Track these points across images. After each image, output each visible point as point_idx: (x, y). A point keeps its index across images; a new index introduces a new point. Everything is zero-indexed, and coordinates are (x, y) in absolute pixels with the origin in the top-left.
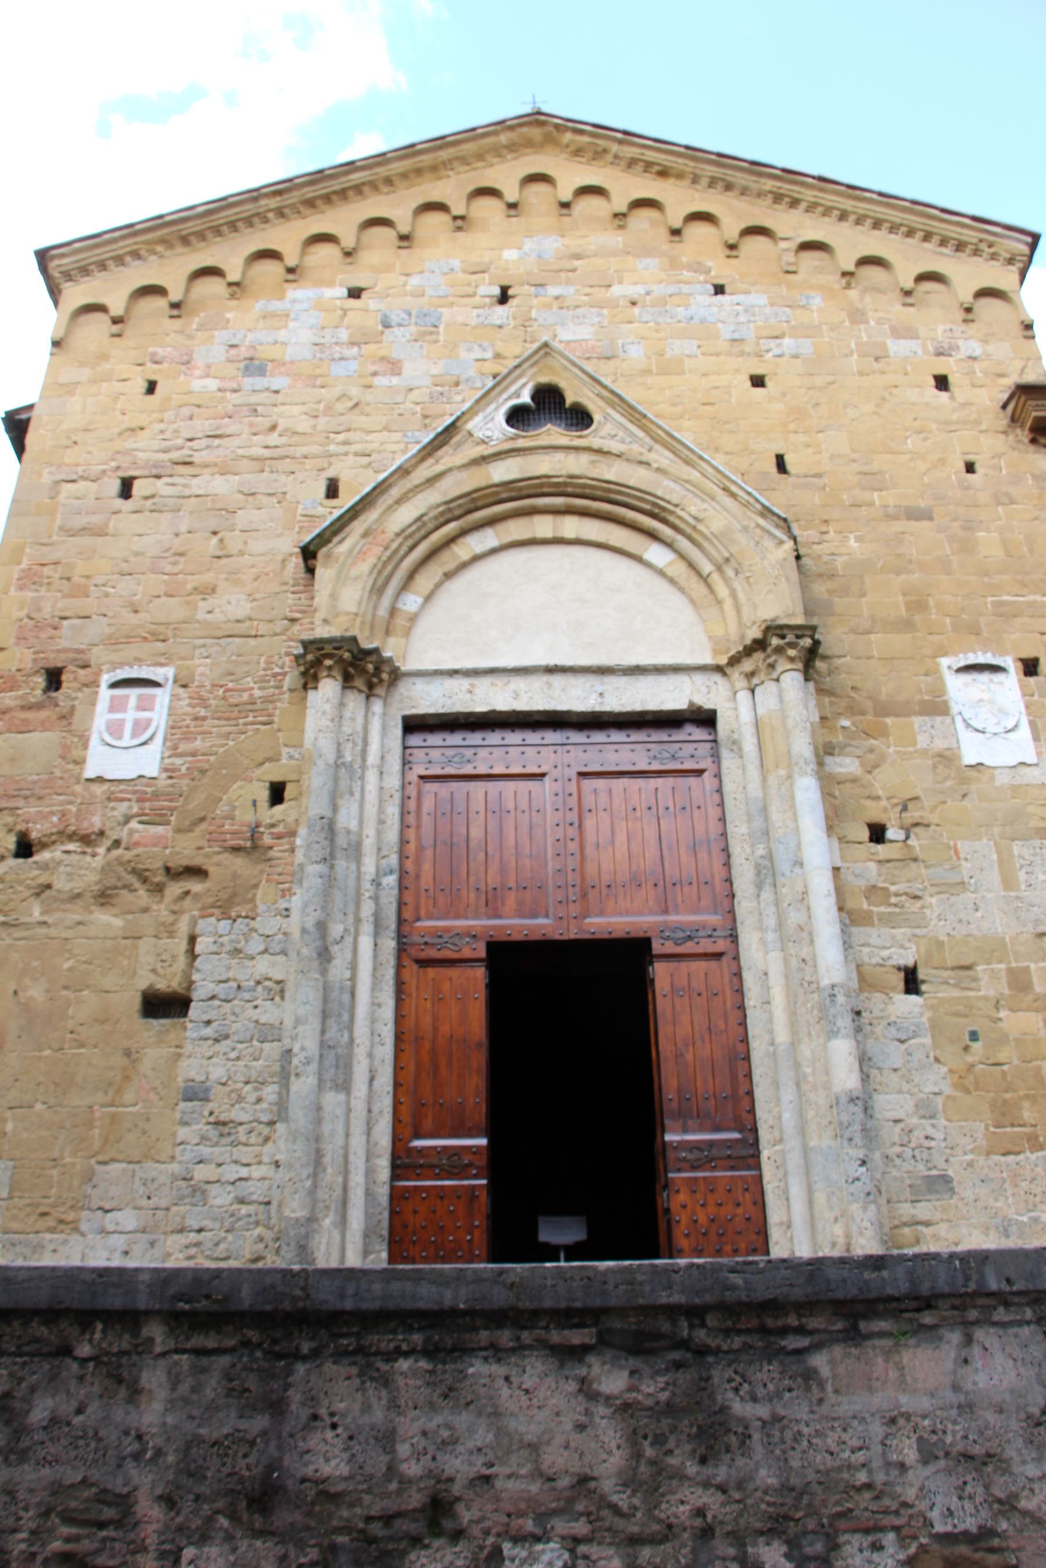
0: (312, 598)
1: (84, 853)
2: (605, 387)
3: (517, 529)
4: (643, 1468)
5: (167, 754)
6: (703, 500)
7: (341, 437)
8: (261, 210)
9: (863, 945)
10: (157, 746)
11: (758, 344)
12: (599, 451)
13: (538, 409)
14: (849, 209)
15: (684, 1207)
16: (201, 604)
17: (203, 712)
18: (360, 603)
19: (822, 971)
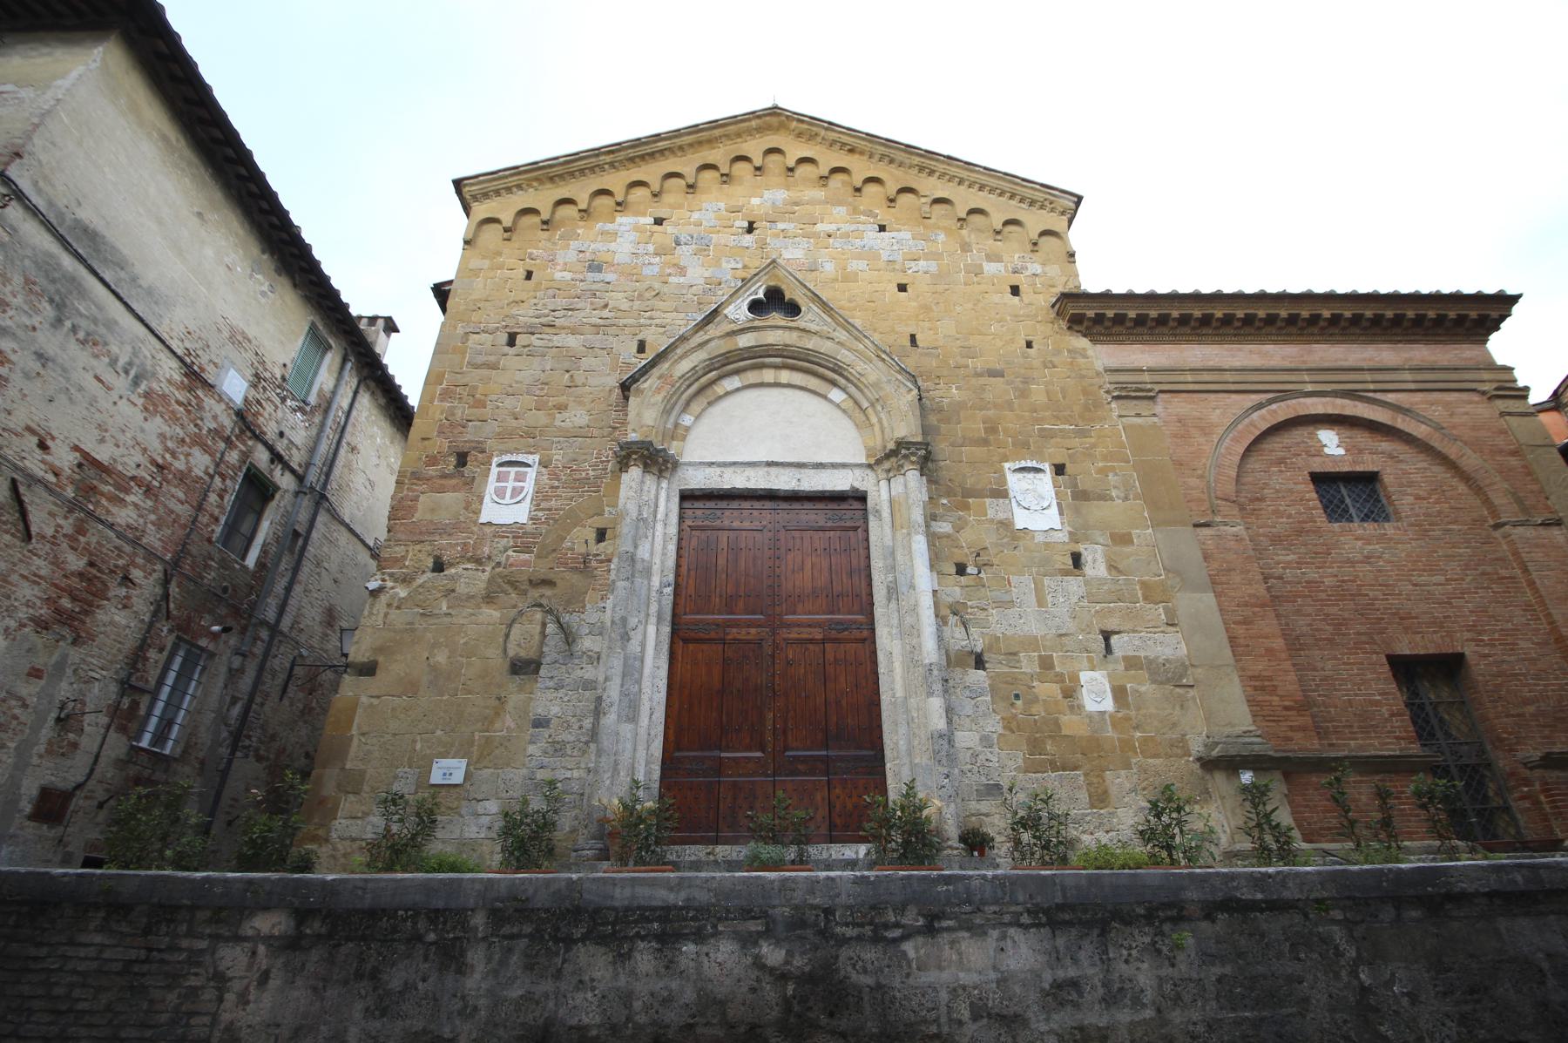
1: (477, 570)
2: (809, 290)
3: (752, 377)
4: (792, 1020)
7: (648, 314)
10: (526, 505)
12: (803, 330)
13: (768, 302)
16: (557, 415)
17: (556, 484)
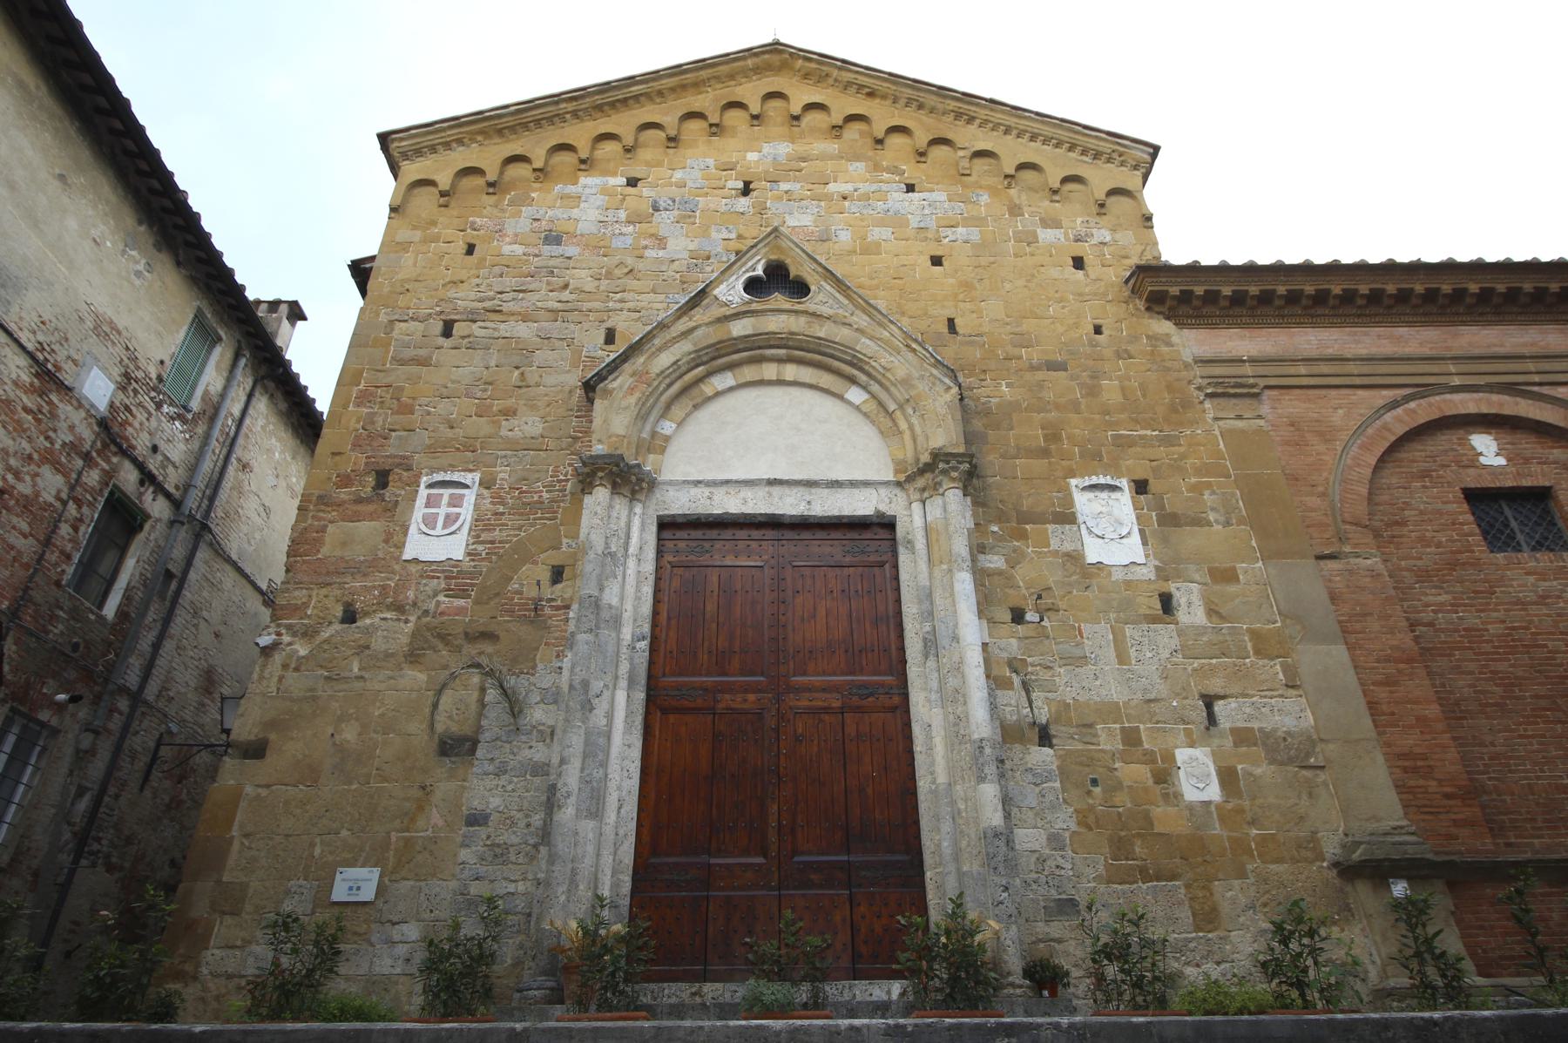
0: (591, 422)
1: (399, 620)
3: (749, 373)
5: (472, 541)
6: (891, 354)
7: (618, 296)
8: (561, 112)
9: (1005, 705)
11: (938, 231)
12: (814, 314)
14: (1013, 125)
15: (863, 917)
17: (501, 509)
18: (627, 427)
19: (973, 727)
